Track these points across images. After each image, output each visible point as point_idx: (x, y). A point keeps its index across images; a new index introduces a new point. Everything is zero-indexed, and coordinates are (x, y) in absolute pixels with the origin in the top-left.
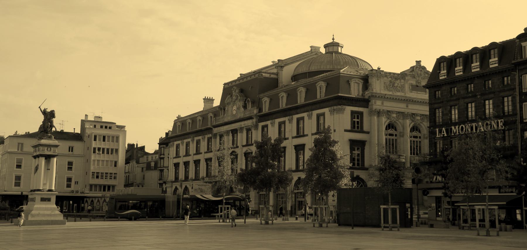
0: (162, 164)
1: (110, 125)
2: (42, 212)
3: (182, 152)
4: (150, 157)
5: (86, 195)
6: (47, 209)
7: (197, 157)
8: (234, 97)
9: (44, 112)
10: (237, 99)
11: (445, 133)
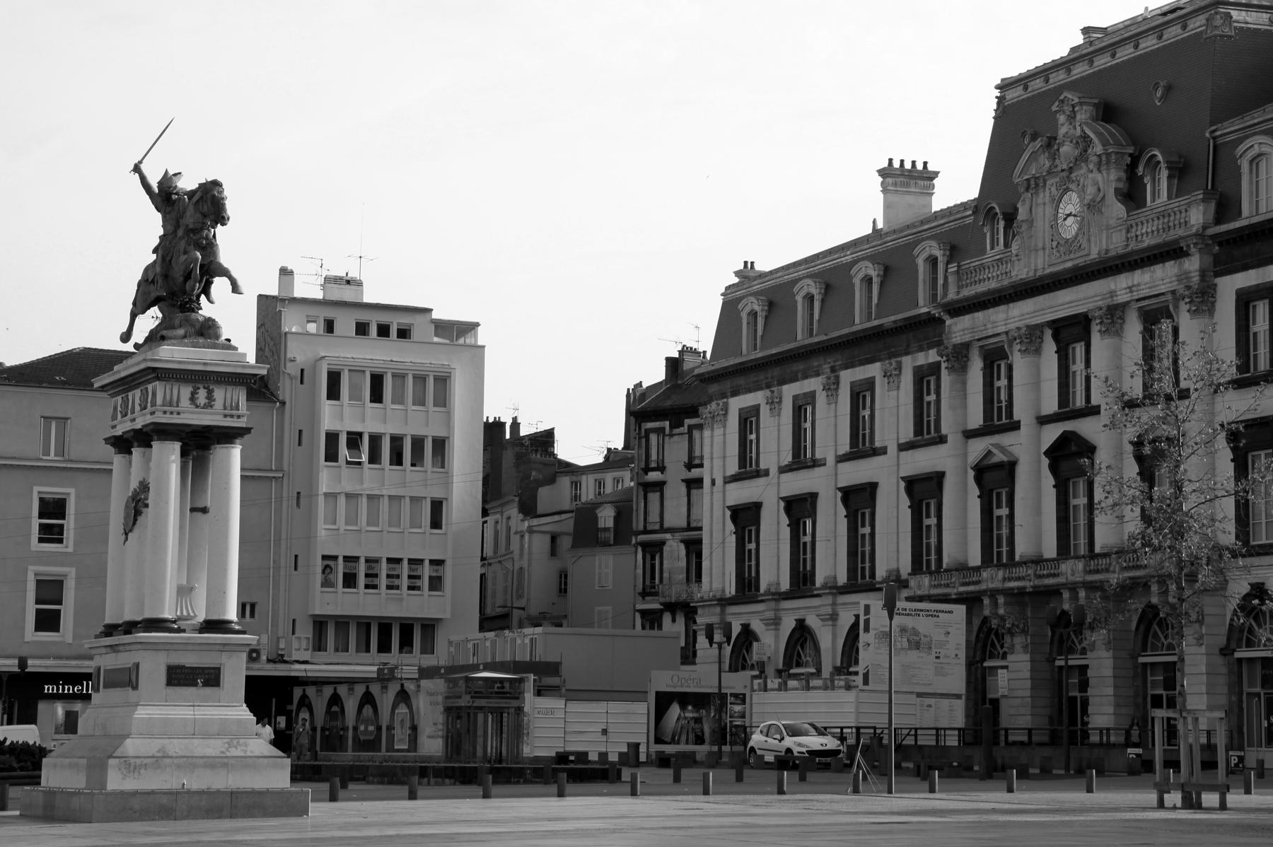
0: (654, 517)
1: (405, 320)
2: (176, 747)
3: (774, 441)
4: (588, 484)
5: (297, 670)
6: (201, 731)
7: (798, 483)
8: (1067, 149)
9: (165, 196)
10: (1082, 158)
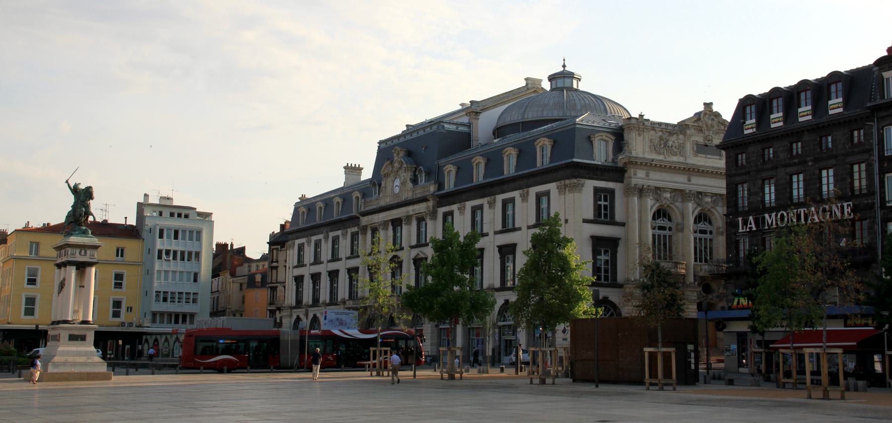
0: (274, 278)
1: (187, 212)
2: (70, 359)
4: (254, 265)
5: (145, 330)
6: (79, 354)
7: (333, 266)
8: (396, 165)
9: (75, 190)
10: (400, 168)
11: (753, 225)
